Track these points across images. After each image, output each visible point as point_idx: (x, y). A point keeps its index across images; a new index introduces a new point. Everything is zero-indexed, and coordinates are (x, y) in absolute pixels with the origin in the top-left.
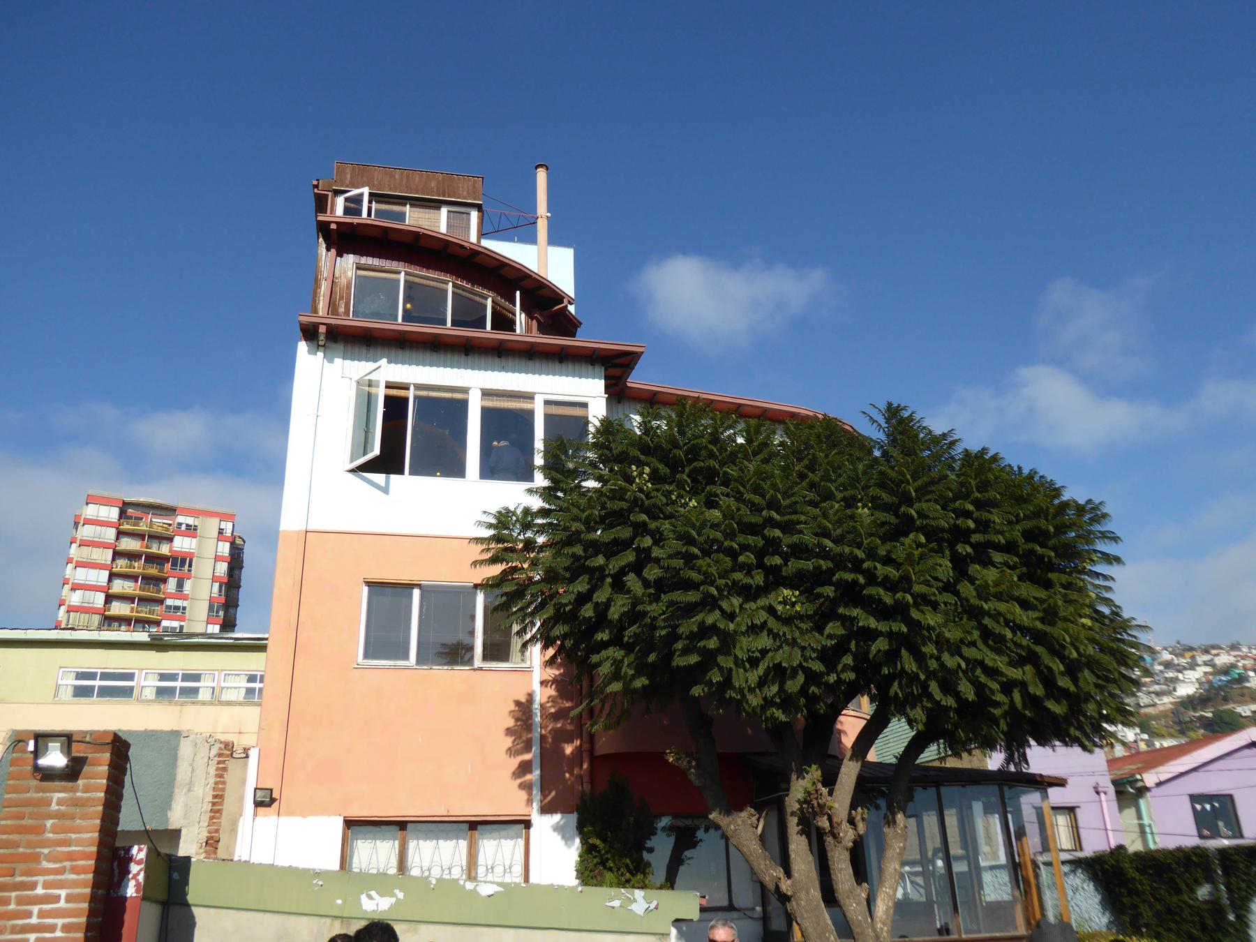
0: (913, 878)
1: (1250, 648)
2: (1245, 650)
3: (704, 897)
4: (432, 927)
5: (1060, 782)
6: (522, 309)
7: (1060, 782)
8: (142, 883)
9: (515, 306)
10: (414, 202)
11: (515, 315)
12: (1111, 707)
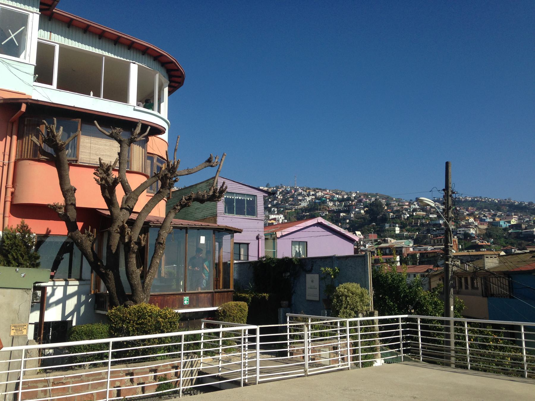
0: (190, 362)
1: (329, 191)
2: (328, 191)
5: (240, 231)
7: (240, 231)
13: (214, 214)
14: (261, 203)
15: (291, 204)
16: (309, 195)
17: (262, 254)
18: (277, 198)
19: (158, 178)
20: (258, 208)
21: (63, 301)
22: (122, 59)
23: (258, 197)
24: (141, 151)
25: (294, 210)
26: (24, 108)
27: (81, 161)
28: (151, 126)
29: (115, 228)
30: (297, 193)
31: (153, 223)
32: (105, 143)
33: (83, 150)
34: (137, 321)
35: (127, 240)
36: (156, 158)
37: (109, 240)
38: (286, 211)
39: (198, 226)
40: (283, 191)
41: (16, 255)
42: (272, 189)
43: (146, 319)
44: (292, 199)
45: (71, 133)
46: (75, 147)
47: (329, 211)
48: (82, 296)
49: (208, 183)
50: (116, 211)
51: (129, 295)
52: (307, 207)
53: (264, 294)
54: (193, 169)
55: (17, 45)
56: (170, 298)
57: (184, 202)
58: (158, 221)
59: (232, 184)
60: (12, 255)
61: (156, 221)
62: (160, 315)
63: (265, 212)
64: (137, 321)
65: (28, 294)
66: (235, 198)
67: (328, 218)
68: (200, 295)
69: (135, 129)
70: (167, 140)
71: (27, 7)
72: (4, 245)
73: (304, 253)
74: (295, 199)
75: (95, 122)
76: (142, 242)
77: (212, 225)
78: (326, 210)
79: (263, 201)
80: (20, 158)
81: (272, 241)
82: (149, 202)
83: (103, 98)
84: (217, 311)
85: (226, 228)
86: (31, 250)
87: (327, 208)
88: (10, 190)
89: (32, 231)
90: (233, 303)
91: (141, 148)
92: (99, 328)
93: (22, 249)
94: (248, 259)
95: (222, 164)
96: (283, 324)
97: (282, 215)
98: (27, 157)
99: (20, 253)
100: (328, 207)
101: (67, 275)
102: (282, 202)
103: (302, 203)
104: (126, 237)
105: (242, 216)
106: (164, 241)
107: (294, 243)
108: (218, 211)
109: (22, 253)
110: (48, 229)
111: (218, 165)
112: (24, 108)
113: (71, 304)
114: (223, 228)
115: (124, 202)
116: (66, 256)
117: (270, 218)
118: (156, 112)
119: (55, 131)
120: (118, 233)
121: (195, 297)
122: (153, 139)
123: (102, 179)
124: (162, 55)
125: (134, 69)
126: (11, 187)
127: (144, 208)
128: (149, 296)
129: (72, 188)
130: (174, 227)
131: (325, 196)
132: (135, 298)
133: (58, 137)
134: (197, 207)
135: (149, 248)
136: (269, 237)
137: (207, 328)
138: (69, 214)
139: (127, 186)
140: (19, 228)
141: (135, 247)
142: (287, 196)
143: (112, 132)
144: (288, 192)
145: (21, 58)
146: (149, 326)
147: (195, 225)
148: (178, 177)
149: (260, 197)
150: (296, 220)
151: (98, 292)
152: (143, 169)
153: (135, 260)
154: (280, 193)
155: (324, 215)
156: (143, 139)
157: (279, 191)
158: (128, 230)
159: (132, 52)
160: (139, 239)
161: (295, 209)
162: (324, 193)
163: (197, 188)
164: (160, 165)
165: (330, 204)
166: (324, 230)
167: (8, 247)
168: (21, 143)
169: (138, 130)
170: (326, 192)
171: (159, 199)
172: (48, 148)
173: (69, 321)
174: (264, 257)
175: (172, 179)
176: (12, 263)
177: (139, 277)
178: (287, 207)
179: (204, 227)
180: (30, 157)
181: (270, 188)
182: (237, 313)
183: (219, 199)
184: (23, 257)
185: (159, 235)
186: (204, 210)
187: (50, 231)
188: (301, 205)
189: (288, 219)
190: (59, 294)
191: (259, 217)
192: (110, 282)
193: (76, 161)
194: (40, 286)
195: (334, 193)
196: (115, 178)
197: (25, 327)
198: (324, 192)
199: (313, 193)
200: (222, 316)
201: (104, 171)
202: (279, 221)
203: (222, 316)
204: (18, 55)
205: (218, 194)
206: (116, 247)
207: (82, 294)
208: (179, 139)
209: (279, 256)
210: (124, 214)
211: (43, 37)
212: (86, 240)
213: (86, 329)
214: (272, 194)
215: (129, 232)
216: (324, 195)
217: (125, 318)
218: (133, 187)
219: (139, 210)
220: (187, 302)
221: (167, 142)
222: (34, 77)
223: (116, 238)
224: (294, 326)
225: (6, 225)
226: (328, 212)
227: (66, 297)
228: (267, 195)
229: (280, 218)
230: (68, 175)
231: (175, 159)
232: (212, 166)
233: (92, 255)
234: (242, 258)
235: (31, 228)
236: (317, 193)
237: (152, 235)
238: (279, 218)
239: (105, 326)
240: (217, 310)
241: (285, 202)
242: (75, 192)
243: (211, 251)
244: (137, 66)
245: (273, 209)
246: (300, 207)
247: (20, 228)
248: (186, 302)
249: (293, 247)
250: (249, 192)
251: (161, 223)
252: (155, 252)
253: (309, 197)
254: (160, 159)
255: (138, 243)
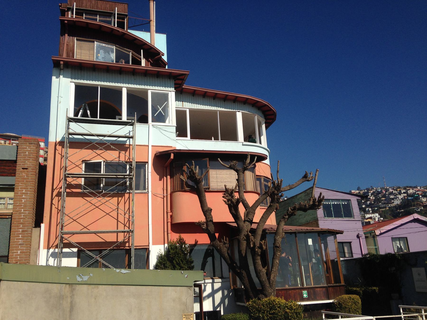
1: (420, 187)
2: (419, 188)
3: (205, 272)
4: (104, 286)
5: (341, 232)
6: (144, 57)
7: (341, 232)
8: (198, 292)
9: (141, 56)
10: (86, 11)
11: (141, 59)
12: (119, 157)
13: (316, 218)
14: (356, 206)
15: (384, 203)
16: (400, 193)
17: (365, 252)
18: (370, 198)
19: (267, 195)
20: (354, 210)
21: (212, 295)
22: (230, 110)
23: (352, 201)
24: (252, 175)
25: (388, 208)
26: (172, 156)
27: (212, 188)
28: (257, 156)
29: (242, 236)
30: (388, 193)
31: (269, 230)
32: (226, 173)
33: (212, 180)
34: (269, 311)
35: (252, 246)
36: (263, 179)
37: (239, 247)
38: (381, 210)
39: (304, 231)
40: (374, 192)
41: (178, 260)
42: (364, 191)
43: (276, 309)
44: (384, 199)
45: (203, 169)
46: (207, 178)
47: (424, 206)
48: (225, 290)
49: (305, 193)
50: (241, 224)
51: (259, 290)
52: (400, 204)
53: (373, 288)
54: (293, 185)
55: (164, 115)
56: (291, 292)
57: (290, 212)
58: (272, 228)
59: (327, 192)
60: (176, 261)
61: (270, 228)
62: (287, 307)
63: (360, 212)
64: (269, 311)
65: (191, 290)
66: (332, 203)
67: (424, 212)
68: (316, 289)
69: (246, 160)
70: (269, 164)
71: (167, 89)
72: (170, 254)
73: (406, 248)
74: (387, 198)
75: (219, 159)
76: (264, 246)
77: (315, 229)
78: (420, 205)
79: (357, 202)
80: (173, 191)
81: (372, 239)
82: (264, 214)
83: (221, 140)
84: (332, 303)
85: (329, 230)
86: (187, 256)
87: (421, 204)
88: (170, 214)
89: (186, 242)
90: (346, 296)
91: (251, 173)
92: (241, 317)
93: (182, 256)
94: (352, 256)
95: (316, 178)
96: (398, 315)
97: (377, 214)
98: (177, 190)
99: (180, 259)
100: (423, 203)
101: (212, 274)
102: (375, 202)
103: (394, 202)
104: (251, 243)
105: (340, 219)
106: (279, 245)
107: (394, 239)
108: (318, 216)
109: (182, 259)
110: (196, 240)
111: (313, 180)
112: (172, 156)
113: (218, 296)
114: (327, 231)
115: (246, 216)
116: (210, 259)
117: (366, 218)
118: (258, 144)
119: (194, 170)
120: (245, 240)
121: (312, 291)
122: (259, 165)
123: (228, 200)
124: (258, 102)
125: (239, 116)
126: (170, 212)
127: (261, 220)
128: (275, 290)
129: (209, 209)
130: (286, 233)
131: (417, 193)
132: (265, 293)
133: (196, 174)
134: (300, 214)
135: (268, 251)
136: (369, 235)
137: (327, 318)
138: (210, 228)
139: (246, 203)
140: (178, 241)
141: (259, 251)
142: (379, 197)
143: (231, 165)
144: (379, 193)
145: (167, 123)
146: (279, 316)
147: (302, 230)
148: (283, 193)
149: (354, 201)
150: (392, 218)
151: (236, 287)
152: (255, 188)
153: (260, 261)
154: (371, 195)
155: (419, 210)
156: (253, 166)
157: (370, 192)
158: (252, 237)
159: (236, 104)
160: (261, 244)
161: (389, 208)
162: (415, 190)
163: (298, 198)
164: (266, 183)
165: (423, 200)
166: (422, 226)
167: (173, 256)
168: (173, 180)
169: (248, 161)
170: (417, 189)
171: (271, 211)
172: (190, 181)
173: (219, 311)
174: (367, 254)
175: (278, 195)
176: (176, 267)
177: (265, 275)
178: (381, 206)
179: (310, 231)
180: (179, 189)
181: (361, 191)
182: (351, 305)
183: (319, 208)
184: (182, 262)
185: (275, 240)
186: (306, 216)
187: (197, 241)
188: (394, 203)
189: (383, 217)
190: (208, 290)
191: (356, 218)
192: (244, 279)
193: (209, 188)
194: (196, 283)
195: (425, 189)
196: (237, 199)
197: (192, 316)
198: (415, 189)
199: (404, 191)
200: (338, 308)
201: (229, 194)
202: (375, 219)
203: (338, 308)
204: (164, 122)
205: (317, 203)
206: (245, 252)
207: (225, 289)
208: (279, 163)
209: (382, 252)
210: (247, 226)
211: (178, 106)
212: (223, 247)
213: (232, 318)
214: (364, 197)
215: (253, 239)
216: (416, 192)
217: (260, 309)
218: (251, 204)
219: (258, 221)
220: (306, 295)
221: (269, 165)
222: (176, 134)
223: (244, 244)
224: (408, 317)
225: (169, 240)
226: (423, 208)
227: (214, 292)
228: (360, 198)
229: (376, 216)
230: (205, 200)
231: (279, 179)
232: (308, 181)
233: (229, 259)
234: (347, 255)
235: (186, 240)
236: (408, 191)
237: (269, 240)
238: (375, 216)
239: (245, 315)
240: (333, 302)
241: (377, 202)
242: (211, 212)
243: (318, 251)
244: (241, 113)
245: (367, 209)
246: (393, 205)
247: (179, 241)
248: (305, 296)
249: (394, 243)
250: (343, 197)
251: (274, 230)
252: (274, 254)
253: (401, 195)
254: (266, 179)
255: (261, 247)
